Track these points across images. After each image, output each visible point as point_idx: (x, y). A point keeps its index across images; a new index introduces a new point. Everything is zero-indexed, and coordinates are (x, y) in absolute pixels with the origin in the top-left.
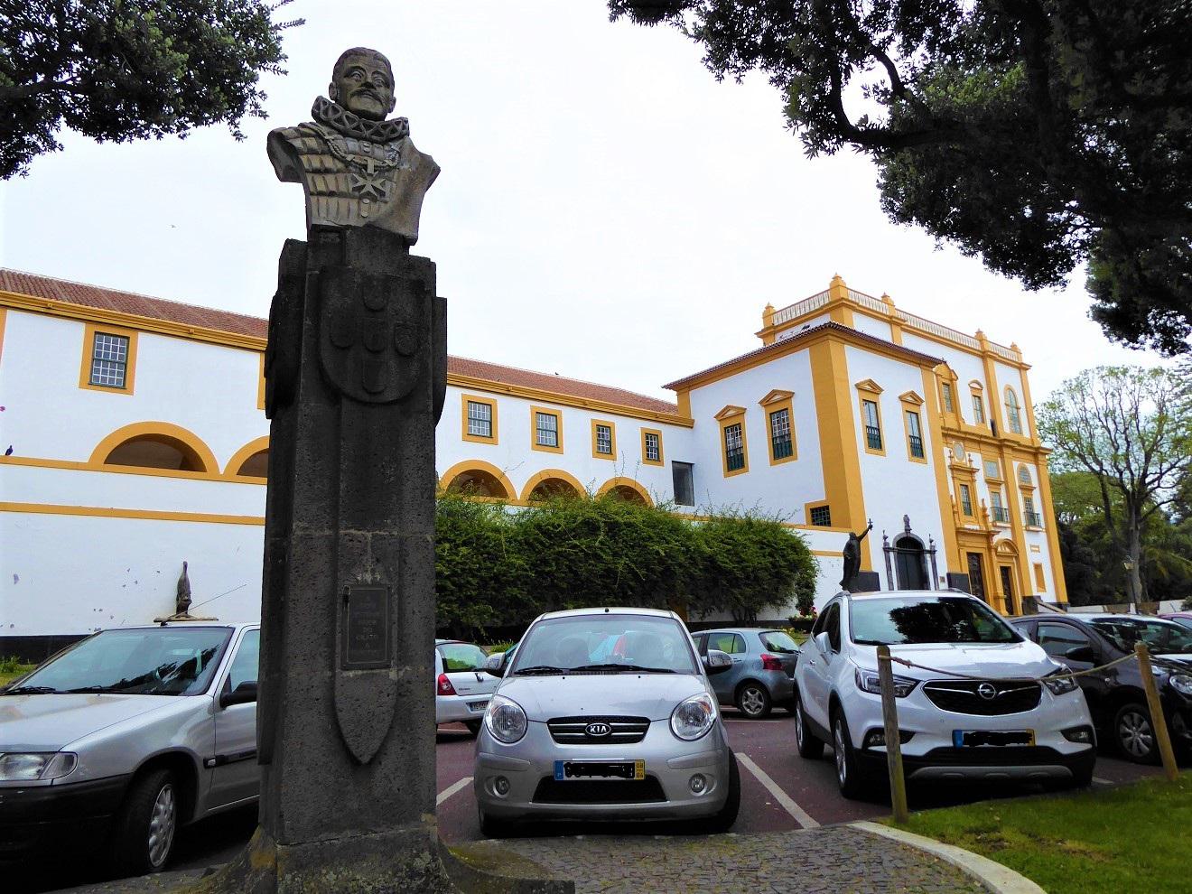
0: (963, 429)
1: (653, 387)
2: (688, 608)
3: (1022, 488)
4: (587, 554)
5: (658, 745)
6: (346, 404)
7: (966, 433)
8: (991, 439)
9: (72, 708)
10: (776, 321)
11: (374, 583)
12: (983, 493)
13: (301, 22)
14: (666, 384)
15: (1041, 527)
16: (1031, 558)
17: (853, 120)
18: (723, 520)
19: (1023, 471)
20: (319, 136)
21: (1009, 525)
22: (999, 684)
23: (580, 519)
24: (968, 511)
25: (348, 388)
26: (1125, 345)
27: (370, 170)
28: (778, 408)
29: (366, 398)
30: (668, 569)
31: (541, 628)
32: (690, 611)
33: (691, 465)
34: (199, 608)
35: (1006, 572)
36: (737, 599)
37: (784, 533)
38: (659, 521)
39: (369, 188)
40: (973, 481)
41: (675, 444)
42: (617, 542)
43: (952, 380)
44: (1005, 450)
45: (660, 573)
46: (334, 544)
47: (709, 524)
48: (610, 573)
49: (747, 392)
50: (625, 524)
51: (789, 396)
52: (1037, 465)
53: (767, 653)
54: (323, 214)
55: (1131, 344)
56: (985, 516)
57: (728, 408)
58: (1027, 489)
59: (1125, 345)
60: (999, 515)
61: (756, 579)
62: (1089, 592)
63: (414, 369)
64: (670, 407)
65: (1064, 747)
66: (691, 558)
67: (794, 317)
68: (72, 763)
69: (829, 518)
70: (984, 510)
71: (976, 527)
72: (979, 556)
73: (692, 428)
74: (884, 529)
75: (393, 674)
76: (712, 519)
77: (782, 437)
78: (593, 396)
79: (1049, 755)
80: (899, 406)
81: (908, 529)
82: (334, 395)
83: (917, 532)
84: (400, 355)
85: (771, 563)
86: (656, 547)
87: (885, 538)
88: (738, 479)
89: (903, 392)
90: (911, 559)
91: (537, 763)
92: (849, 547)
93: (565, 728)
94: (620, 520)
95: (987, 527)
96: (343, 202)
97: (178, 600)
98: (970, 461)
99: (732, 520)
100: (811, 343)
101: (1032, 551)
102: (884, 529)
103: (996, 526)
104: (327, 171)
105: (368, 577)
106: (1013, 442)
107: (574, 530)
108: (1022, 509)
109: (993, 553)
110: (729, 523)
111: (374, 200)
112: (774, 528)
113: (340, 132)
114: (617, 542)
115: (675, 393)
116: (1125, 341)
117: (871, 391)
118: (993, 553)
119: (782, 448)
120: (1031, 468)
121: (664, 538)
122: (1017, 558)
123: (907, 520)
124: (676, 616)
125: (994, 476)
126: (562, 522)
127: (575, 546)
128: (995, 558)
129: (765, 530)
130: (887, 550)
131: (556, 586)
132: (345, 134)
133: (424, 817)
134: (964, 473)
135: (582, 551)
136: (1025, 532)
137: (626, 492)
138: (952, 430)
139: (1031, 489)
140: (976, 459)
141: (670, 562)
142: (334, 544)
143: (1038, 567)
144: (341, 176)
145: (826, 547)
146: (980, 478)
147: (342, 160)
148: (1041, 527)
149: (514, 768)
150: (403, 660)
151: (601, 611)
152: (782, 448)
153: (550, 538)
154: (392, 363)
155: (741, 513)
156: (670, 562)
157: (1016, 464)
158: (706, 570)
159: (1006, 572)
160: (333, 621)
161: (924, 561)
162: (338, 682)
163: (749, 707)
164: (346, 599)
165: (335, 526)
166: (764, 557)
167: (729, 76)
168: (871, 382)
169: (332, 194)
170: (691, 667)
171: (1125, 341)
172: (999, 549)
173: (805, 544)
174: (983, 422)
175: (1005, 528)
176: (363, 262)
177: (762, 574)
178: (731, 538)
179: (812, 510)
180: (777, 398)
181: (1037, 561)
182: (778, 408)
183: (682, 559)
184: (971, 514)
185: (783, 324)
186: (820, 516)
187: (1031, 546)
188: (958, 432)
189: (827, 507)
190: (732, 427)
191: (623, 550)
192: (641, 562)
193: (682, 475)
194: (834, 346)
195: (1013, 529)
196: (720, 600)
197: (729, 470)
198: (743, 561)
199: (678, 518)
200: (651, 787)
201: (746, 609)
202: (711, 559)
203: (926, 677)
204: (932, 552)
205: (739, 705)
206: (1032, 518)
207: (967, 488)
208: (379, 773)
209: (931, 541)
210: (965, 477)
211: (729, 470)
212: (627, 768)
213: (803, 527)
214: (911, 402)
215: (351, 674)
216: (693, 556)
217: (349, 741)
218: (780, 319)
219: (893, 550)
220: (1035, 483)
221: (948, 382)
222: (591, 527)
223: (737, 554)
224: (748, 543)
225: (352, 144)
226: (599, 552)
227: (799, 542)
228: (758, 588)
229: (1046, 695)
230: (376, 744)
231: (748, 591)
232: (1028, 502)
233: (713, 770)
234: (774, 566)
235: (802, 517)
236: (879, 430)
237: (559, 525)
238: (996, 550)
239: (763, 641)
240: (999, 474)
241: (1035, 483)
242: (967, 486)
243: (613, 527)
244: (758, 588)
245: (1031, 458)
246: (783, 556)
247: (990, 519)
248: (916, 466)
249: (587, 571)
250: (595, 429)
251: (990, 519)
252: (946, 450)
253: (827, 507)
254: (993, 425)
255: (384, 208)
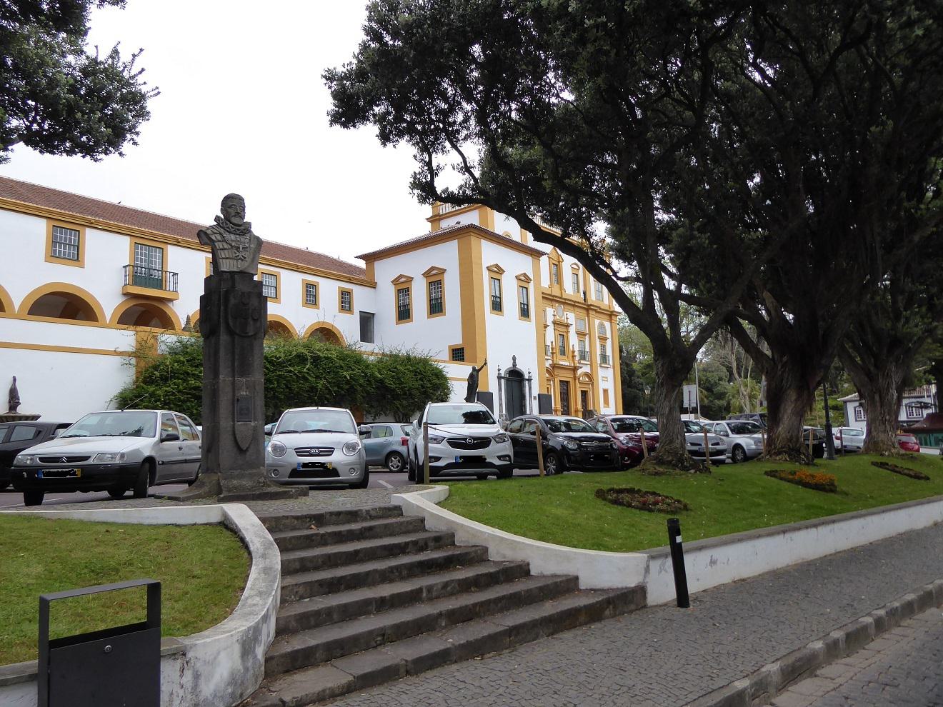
0: (564, 297)
1: (349, 254)
2: (365, 413)
3: (600, 338)
4: (298, 377)
5: (337, 458)
6: (237, 337)
7: (565, 299)
8: (583, 304)
9: (96, 441)
10: (441, 211)
11: (246, 395)
12: (573, 340)
13: (143, 70)
14: (358, 255)
15: (609, 364)
16: (602, 385)
17: (439, 190)
18: (391, 356)
19: (602, 326)
20: (220, 234)
21: (589, 363)
22: (475, 438)
23: (294, 353)
24: (563, 353)
25: (237, 331)
26: (626, 266)
27: (241, 248)
28: (435, 280)
29: (243, 335)
30: (352, 387)
31: (287, 415)
32: (366, 415)
33: (373, 314)
34: (22, 410)
35: (584, 393)
36: (398, 408)
37: (431, 365)
38: (347, 355)
39: (240, 256)
40: (568, 332)
41: (362, 299)
42: (318, 369)
43: (559, 262)
44: (591, 312)
45: (347, 390)
46: (233, 383)
47: (381, 358)
48: (313, 389)
49: (415, 266)
50: (325, 357)
51: (442, 271)
52: (611, 323)
53: (405, 436)
54: (225, 266)
55: (629, 266)
56: (574, 356)
57: (401, 276)
58: (603, 339)
59: (626, 266)
60: (583, 357)
61: (411, 395)
62: (639, 409)
63: (258, 324)
64: (360, 270)
65: (497, 462)
66: (368, 381)
67: (447, 211)
68: (123, 457)
69: (463, 356)
70: (573, 352)
71: (567, 364)
72: (567, 382)
73: (375, 288)
74: (496, 364)
75: (252, 424)
76: (384, 355)
77: (436, 299)
78: (304, 261)
79: (491, 465)
80: (515, 283)
81: (514, 365)
82: (231, 333)
83: (520, 367)
84: (254, 320)
85: (421, 385)
86: (345, 373)
87: (499, 370)
88: (406, 326)
89: (518, 273)
90: (515, 384)
91: (291, 464)
92: (471, 376)
93: (300, 451)
94: (321, 355)
95: (574, 363)
96: (231, 261)
97: (10, 402)
98: (567, 318)
99: (397, 356)
100: (458, 237)
101: (603, 380)
102: (496, 364)
103: (580, 363)
104: (226, 249)
105: (245, 393)
106: (596, 306)
107: (290, 360)
108: (599, 352)
109: (577, 381)
110: (395, 358)
111: (242, 260)
112: (425, 362)
113: (228, 231)
114: (318, 369)
115: (364, 262)
116: (626, 264)
117: (497, 271)
118: (577, 381)
119: (436, 307)
120: (607, 325)
121: (350, 367)
122: (592, 385)
123: (514, 359)
124: (348, 411)
125: (582, 330)
126: (283, 355)
127: (290, 371)
128: (578, 385)
129: (418, 363)
130: (500, 378)
131: (278, 398)
132: (230, 232)
133: (261, 468)
134: (561, 326)
135: (295, 374)
136: (599, 368)
137: (326, 333)
138: (556, 297)
139: (606, 339)
140: (571, 317)
141: (354, 383)
142: (233, 383)
143: (605, 391)
144: (230, 251)
145: (457, 374)
146: (572, 330)
147: (231, 245)
148: (609, 364)
149: (282, 466)
150: (255, 420)
151: (316, 408)
152: (436, 307)
153: (273, 365)
154: (251, 323)
155: (404, 352)
156: (354, 383)
157: (597, 322)
158: (377, 388)
159: (584, 393)
160: (234, 407)
161: (524, 386)
162: (236, 425)
163: (392, 466)
164: (238, 400)
165: (234, 377)
166: (417, 380)
167: (390, 145)
168: (497, 266)
169: (227, 258)
170: (353, 430)
171: (626, 264)
172: (581, 379)
173: (444, 373)
174: (578, 292)
175: (586, 364)
176: (241, 286)
177: (414, 392)
178: (396, 368)
179: (453, 350)
180: (435, 272)
181: (605, 387)
182: (435, 280)
183: (362, 381)
184: (564, 355)
185: (446, 214)
186: (458, 354)
187: (603, 377)
188: (560, 298)
189: (463, 349)
190: (403, 287)
191: (322, 374)
192: (334, 383)
193: (367, 321)
194: (474, 240)
195: (591, 365)
196: (387, 408)
197: (399, 320)
198: (402, 383)
199: (360, 354)
200: (334, 472)
201: (403, 414)
202: (381, 381)
203: (448, 436)
204: (529, 380)
205: (388, 467)
206: (604, 358)
207: (563, 337)
208: (248, 453)
209: (529, 373)
210: (563, 329)
211: (399, 320)
212: (322, 465)
213: (445, 362)
214: (523, 280)
215: (240, 423)
216: (369, 379)
217: (239, 440)
218: (444, 210)
219: (503, 378)
220: (609, 335)
221: (557, 263)
222: (301, 359)
223: (399, 378)
224: (406, 371)
225: (233, 237)
226: (307, 375)
227: (441, 371)
228: (411, 401)
229: (493, 442)
230: (247, 445)
231: (405, 402)
232: (603, 347)
233: (358, 466)
234: (423, 387)
235: (446, 355)
236: (500, 298)
237: (280, 358)
238: (579, 379)
239: (403, 430)
240: (585, 328)
241: (609, 335)
242: (563, 335)
243: (316, 359)
244: (411, 401)
245: (607, 317)
246: (430, 381)
247: (577, 358)
248: (524, 323)
249: (298, 387)
250: (305, 286)
251: (577, 358)
252: (550, 311)
253: (463, 349)
254: (584, 294)
255: (246, 264)
